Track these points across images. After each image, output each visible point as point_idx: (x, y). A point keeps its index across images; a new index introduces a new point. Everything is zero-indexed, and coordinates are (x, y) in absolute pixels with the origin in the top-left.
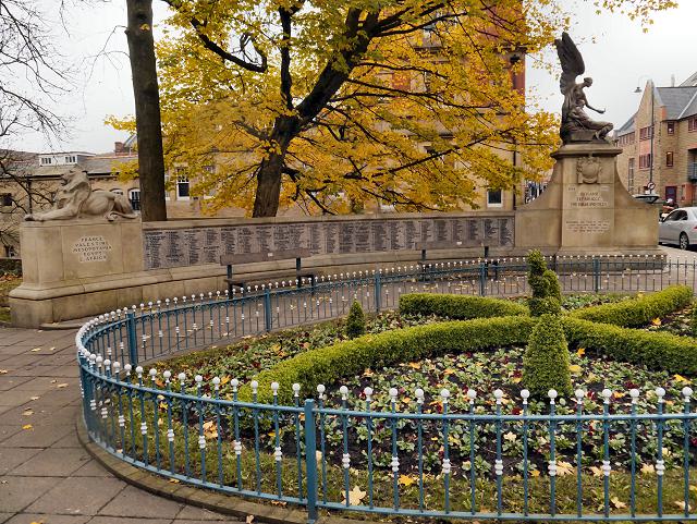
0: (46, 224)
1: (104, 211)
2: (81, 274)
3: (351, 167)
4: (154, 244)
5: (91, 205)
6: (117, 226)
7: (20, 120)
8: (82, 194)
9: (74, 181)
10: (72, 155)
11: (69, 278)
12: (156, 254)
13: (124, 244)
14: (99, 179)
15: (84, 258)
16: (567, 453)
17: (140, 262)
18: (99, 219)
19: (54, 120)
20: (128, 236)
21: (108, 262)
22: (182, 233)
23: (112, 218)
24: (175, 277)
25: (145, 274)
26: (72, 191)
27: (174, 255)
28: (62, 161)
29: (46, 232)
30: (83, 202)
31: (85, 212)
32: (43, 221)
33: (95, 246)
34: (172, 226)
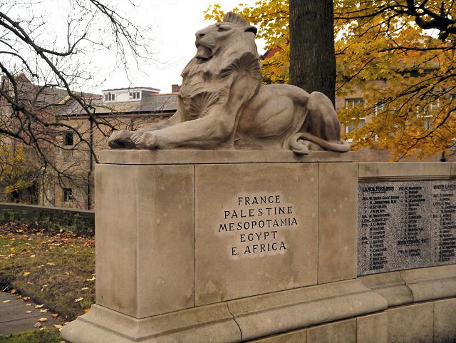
0: (162, 156)
1: (285, 130)
2: (233, 290)
3: (85, 165)
4: (376, 216)
5: (262, 114)
6: (312, 170)
7: (91, 37)
8: (245, 84)
9: (230, 50)
10: (136, 91)
11: (208, 299)
12: (378, 243)
13: (323, 214)
14: (145, 118)
15: (241, 247)
16: (45, 171)
17: (350, 256)
18: (276, 151)
19: (131, 30)
20: (330, 194)
21: (289, 258)
22: (429, 191)
23: (303, 146)
24: (419, 292)
25: (357, 285)
26: (225, 73)
27: (412, 240)
28: (123, 98)
29: (162, 177)
30: (245, 106)
31: (247, 132)
32: (155, 148)
33: (265, 217)
34: (412, 174)
